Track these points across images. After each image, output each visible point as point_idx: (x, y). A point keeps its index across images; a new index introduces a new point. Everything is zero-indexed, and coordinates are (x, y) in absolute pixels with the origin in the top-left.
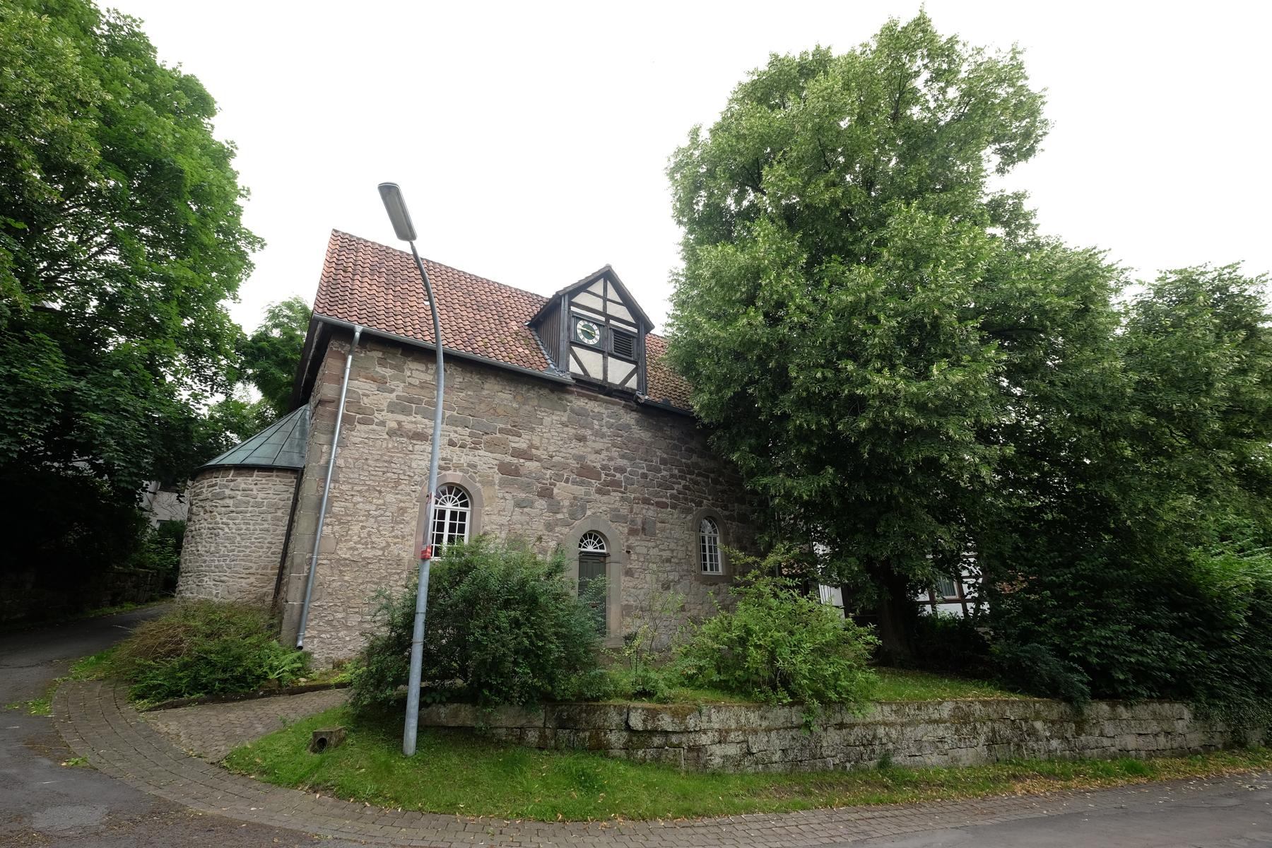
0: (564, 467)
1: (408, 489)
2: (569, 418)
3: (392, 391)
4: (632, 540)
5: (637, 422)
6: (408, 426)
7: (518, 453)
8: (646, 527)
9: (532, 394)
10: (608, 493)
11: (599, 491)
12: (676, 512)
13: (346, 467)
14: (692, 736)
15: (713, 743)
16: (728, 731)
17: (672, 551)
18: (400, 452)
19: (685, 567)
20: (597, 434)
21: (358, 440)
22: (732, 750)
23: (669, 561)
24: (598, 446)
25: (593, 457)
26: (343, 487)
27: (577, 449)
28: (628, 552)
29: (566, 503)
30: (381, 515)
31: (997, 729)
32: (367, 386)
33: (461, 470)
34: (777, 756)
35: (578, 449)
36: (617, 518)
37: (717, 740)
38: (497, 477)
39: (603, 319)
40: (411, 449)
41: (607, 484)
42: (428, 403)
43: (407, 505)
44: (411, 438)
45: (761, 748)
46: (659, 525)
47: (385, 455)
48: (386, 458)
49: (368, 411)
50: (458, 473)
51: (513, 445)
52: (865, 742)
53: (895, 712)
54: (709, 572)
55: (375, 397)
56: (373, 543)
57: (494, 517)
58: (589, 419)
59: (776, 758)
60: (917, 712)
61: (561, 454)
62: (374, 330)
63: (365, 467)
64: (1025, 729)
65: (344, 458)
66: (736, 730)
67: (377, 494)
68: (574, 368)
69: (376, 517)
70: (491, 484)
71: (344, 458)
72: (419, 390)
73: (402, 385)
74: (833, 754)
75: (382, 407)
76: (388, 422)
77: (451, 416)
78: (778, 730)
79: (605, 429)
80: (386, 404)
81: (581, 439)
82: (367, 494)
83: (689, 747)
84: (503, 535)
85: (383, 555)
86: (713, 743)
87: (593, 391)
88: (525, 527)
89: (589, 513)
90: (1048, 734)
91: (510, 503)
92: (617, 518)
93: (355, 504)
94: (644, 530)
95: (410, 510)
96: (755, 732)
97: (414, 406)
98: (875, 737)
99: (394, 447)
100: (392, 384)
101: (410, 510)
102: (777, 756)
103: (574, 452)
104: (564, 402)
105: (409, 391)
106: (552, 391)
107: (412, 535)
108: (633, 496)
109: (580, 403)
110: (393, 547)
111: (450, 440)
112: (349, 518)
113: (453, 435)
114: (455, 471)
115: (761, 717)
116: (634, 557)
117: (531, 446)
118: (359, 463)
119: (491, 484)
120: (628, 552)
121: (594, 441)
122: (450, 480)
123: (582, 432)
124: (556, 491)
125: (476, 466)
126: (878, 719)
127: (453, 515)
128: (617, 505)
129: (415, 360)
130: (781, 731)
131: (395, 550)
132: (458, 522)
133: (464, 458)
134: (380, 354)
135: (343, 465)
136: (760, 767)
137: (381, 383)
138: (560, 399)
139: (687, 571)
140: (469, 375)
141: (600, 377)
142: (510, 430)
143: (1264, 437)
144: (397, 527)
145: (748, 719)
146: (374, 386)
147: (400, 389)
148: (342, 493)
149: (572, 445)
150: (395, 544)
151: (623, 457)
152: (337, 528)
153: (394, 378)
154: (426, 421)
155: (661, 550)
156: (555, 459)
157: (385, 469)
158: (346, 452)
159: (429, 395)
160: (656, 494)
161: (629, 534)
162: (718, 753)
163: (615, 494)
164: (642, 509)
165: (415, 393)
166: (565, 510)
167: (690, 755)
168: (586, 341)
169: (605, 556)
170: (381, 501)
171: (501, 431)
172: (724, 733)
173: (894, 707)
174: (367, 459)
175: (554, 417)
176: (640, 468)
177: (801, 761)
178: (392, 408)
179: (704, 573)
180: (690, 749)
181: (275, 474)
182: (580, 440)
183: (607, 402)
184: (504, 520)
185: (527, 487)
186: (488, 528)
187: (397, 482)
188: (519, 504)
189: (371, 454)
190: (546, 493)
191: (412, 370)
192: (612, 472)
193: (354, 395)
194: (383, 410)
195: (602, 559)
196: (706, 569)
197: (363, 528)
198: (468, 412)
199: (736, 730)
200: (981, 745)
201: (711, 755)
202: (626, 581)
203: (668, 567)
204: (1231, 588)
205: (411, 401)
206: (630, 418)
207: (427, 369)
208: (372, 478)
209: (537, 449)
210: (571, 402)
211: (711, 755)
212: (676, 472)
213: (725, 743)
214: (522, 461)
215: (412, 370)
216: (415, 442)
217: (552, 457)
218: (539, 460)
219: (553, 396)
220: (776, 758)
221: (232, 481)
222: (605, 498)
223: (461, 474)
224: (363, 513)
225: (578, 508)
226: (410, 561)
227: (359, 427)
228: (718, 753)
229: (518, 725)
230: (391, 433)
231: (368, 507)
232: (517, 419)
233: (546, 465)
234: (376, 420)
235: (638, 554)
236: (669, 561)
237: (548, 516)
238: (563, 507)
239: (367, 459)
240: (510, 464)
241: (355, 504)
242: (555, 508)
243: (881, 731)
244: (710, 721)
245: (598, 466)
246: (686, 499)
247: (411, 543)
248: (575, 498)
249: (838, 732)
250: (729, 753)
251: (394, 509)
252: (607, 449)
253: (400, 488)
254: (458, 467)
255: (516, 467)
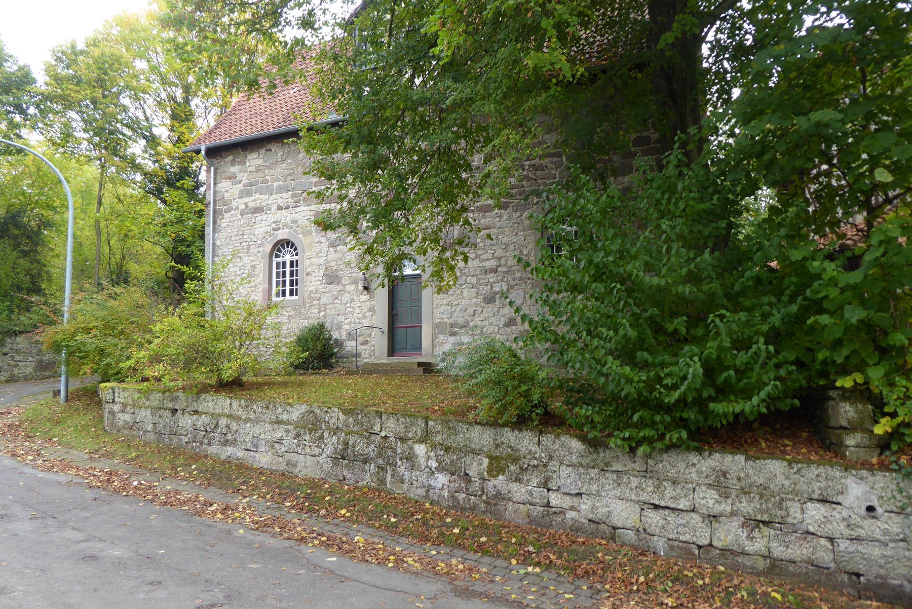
12: (505, 214)
17: (500, 259)
31: (351, 443)
44: (253, 213)
64: (399, 451)
67: (238, 259)
88: (339, 263)
90: (434, 464)
91: (325, 246)
122: (280, 238)
126: (225, 411)
132: (281, 270)
137: (232, 178)
153: (241, 171)
155: (482, 261)
187: (249, 248)
198: (289, 178)
200: (324, 456)
203: (492, 277)
227: (226, 215)
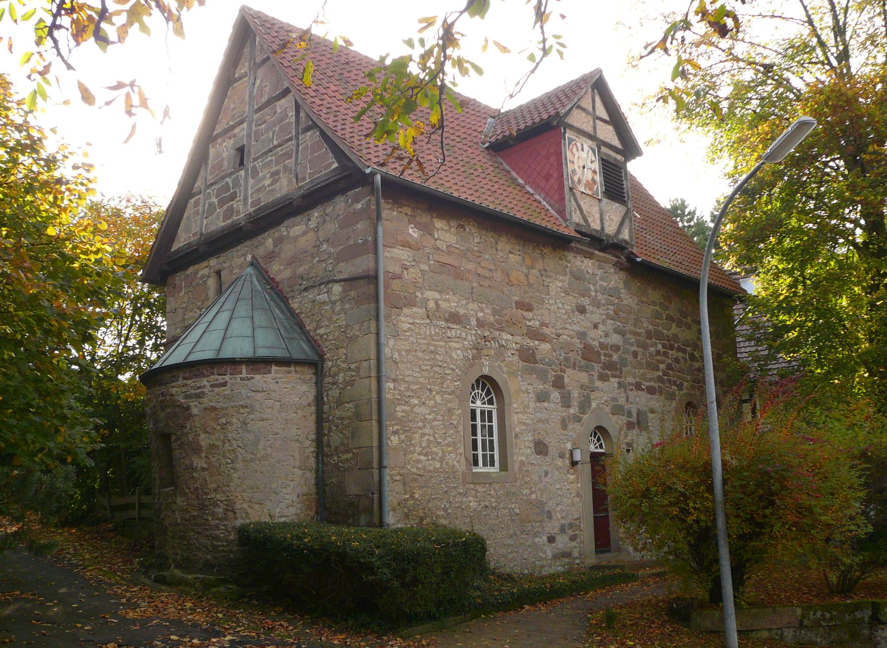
24: (596, 318)
27: (580, 323)
54: (480, 469)
81: (582, 310)
89: (594, 405)
109: (586, 265)
134: (408, 210)
141: (598, 228)
179: (475, 470)
181: (292, 368)
189: (420, 344)
196: (476, 463)
204: (691, 74)
206: (616, 279)
212: (660, 347)
214: (537, 342)
221: (248, 379)
226: (463, 473)
246: (669, 381)
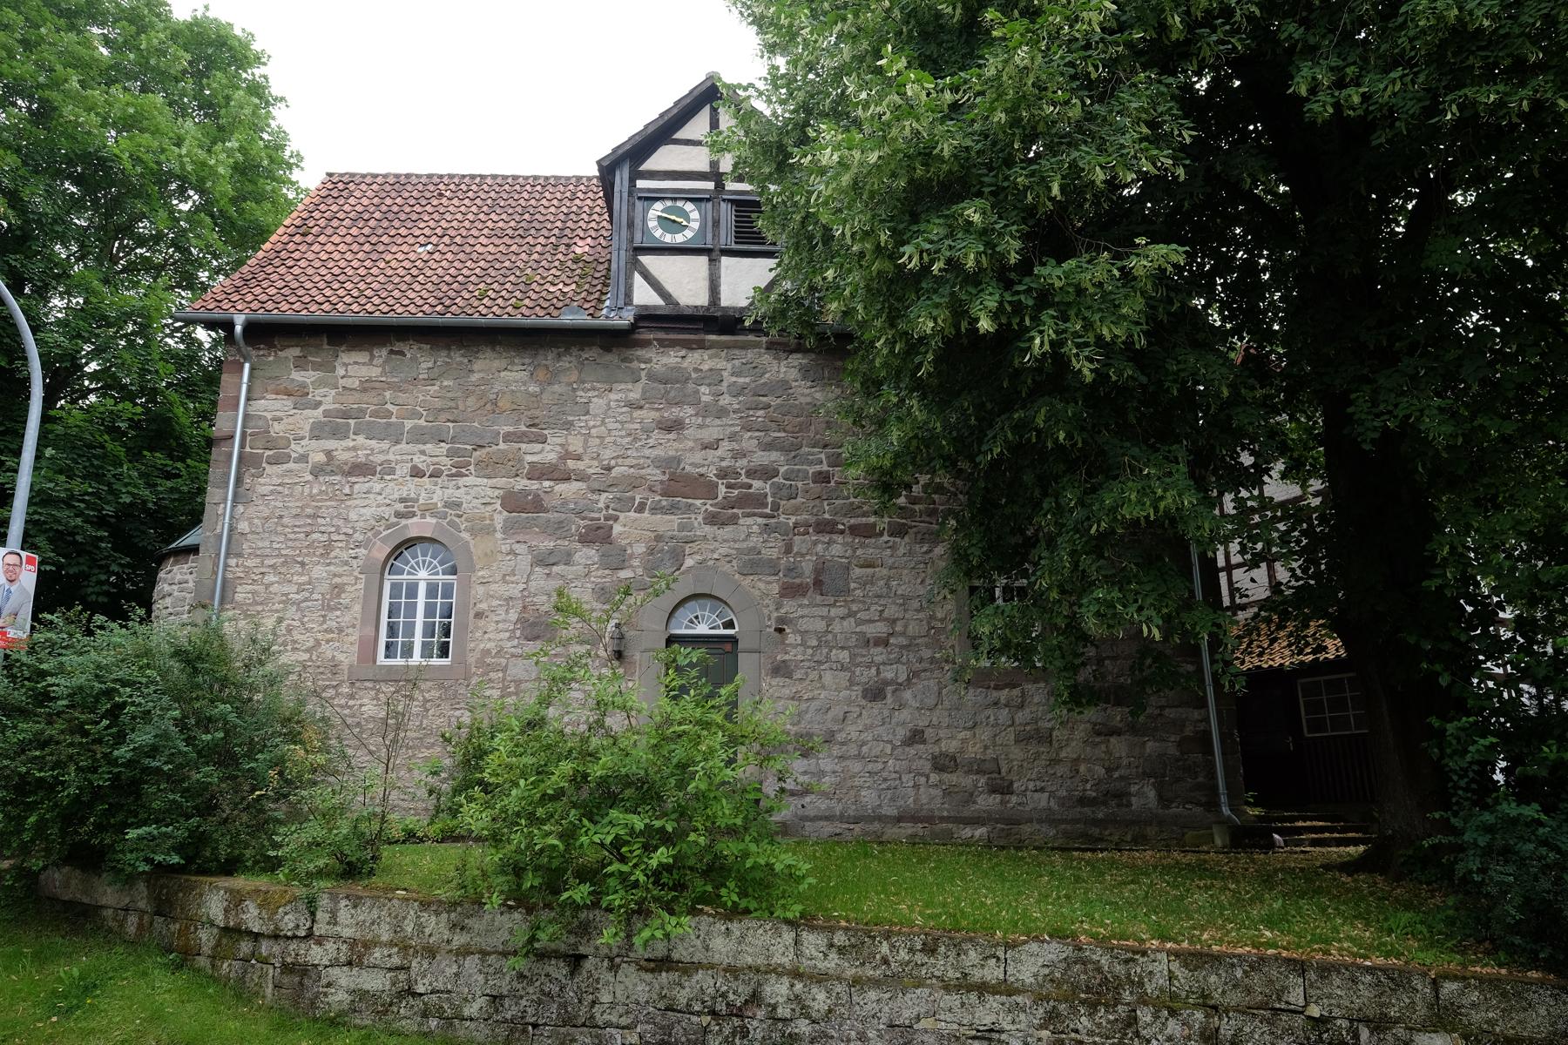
0: (634, 483)
1: (345, 555)
2: (644, 392)
3: (318, 404)
4: (789, 606)
5: (805, 372)
6: (342, 456)
7: (540, 472)
8: (825, 578)
9: (565, 362)
10: (733, 520)
11: (712, 519)
12: (903, 545)
13: (253, 532)
14: (293, 946)
15: (334, 963)
16: (368, 945)
18: (330, 499)
19: (926, 653)
20: (705, 411)
21: (265, 490)
22: (375, 982)
23: (883, 642)
25: (698, 457)
26: (249, 563)
28: (780, 630)
29: (640, 549)
30: (306, 600)
32: (278, 405)
33: (433, 515)
34: (476, 1006)
35: (666, 445)
36: (754, 565)
37: (343, 959)
38: (500, 518)
39: (710, 185)
40: (347, 490)
41: (730, 504)
42: (375, 414)
43: (345, 579)
44: (350, 474)
45: (440, 986)
46: (858, 571)
47: (308, 506)
48: (309, 511)
49: (282, 443)
50: (429, 520)
51: (529, 458)
52: (721, 1007)
53: (841, 951)
55: (291, 419)
56: (295, 642)
57: (494, 587)
58: (691, 386)
59: (472, 1009)
60: (919, 958)
61: (627, 462)
62: (261, 315)
63: (280, 528)
65: (249, 519)
66: (391, 944)
67: (298, 568)
68: (644, 295)
69: (298, 603)
70: (489, 531)
71: (249, 519)
72: (357, 395)
73: (333, 392)
74: (624, 1021)
75: (302, 433)
76: (312, 455)
77: (415, 427)
78: (484, 954)
79: (725, 400)
80: (307, 427)
81: (673, 426)
82: (283, 570)
83: (284, 965)
84: (513, 616)
85: (310, 659)
86: (334, 963)
87: (696, 331)
89: (689, 562)
91: (524, 561)
92: (754, 565)
93: (267, 586)
94: (823, 583)
95: (349, 588)
96: (431, 952)
97: (352, 422)
98: (755, 998)
99: (321, 492)
100: (316, 394)
101: (349, 588)
102: (476, 1006)
103: (659, 452)
104: (635, 364)
105: (343, 399)
106: (607, 349)
107: (354, 626)
108: (793, 519)
109: (669, 359)
110: (324, 646)
111: (414, 468)
112: (259, 608)
113: (419, 460)
114: (423, 516)
115: (453, 926)
116: (792, 638)
117: (567, 455)
118: (270, 524)
119: (489, 531)
120: (780, 630)
121: (700, 427)
123: (676, 412)
124: (617, 529)
125: (459, 505)
127: (432, 591)
128: (755, 541)
129: (353, 347)
130: (492, 959)
131: (327, 651)
133: (436, 493)
134: (296, 351)
135: (247, 530)
136: (433, 1023)
137: (299, 395)
138: (624, 360)
139: (932, 660)
140: (444, 353)
141: (702, 299)
142: (524, 433)
143: (239, 40)
144: (330, 615)
145: (420, 928)
146: (288, 403)
147: (330, 399)
148: (248, 570)
149: (652, 442)
150: (328, 641)
151: (768, 447)
152: (242, 624)
153: (320, 383)
154: (373, 442)
156: (614, 472)
157: (308, 529)
158: (251, 510)
159: (375, 400)
160: (852, 510)
161: (782, 595)
162: (342, 985)
163: (750, 521)
164: (815, 543)
165: (352, 403)
166: (636, 563)
167: (286, 980)
168: (668, 239)
169: (733, 640)
170: (305, 579)
171: (508, 438)
172: (360, 948)
173: (840, 938)
174: (281, 517)
175: (613, 396)
176: (811, 463)
177: (535, 1026)
178: (318, 432)
180: (287, 968)
182: (669, 430)
183: (727, 346)
184: (515, 590)
185: (558, 529)
186: (484, 606)
187: (328, 547)
188: (543, 560)
189: (287, 508)
190: (598, 535)
191: (346, 365)
192: (744, 479)
193: (260, 423)
194: (302, 438)
195: (728, 647)
197: (280, 620)
198: (443, 416)
199: (391, 944)
201: (329, 985)
202: (772, 685)
203: (879, 654)
205: (346, 415)
206: (787, 369)
207: (372, 357)
208: (290, 544)
209: (579, 458)
210: (648, 361)
211: (329, 985)
213: (360, 965)
214: (547, 484)
215: (346, 365)
216: (354, 479)
217: (609, 469)
218: (582, 477)
219: (609, 357)
220: (472, 1009)
222: (727, 532)
223: (434, 521)
224: (278, 598)
225: (667, 552)
227: (269, 469)
228: (343, 982)
229: (122, 905)
230: (317, 471)
231: (286, 589)
232: (537, 413)
233: (596, 486)
234: (294, 455)
235: (804, 633)
236: (883, 642)
237: (600, 576)
238: (631, 556)
239: (281, 517)
240: (525, 493)
241: (267, 586)
242: (616, 560)
243: (778, 990)
244: (333, 921)
245: (711, 473)
247: (351, 639)
248: (658, 538)
249: (648, 977)
250: (366, 987)
251: (325, 587)
252: (732, 437)
253: (333, 554)
254: (429, 510)
255: (537, 496)
